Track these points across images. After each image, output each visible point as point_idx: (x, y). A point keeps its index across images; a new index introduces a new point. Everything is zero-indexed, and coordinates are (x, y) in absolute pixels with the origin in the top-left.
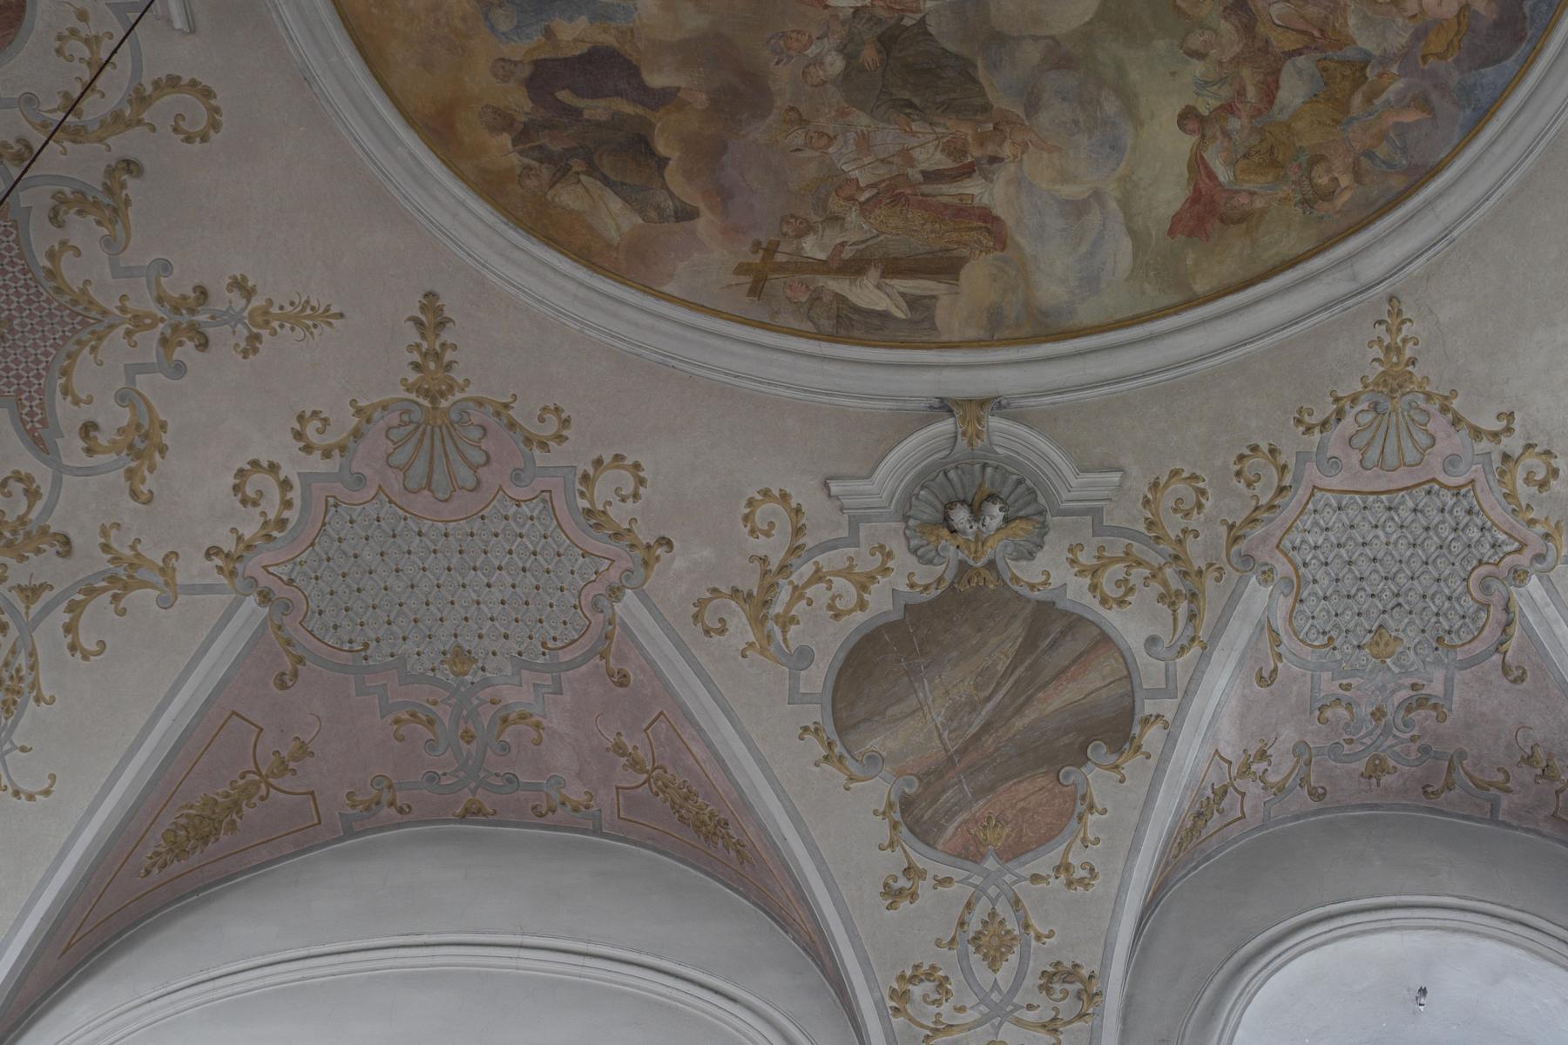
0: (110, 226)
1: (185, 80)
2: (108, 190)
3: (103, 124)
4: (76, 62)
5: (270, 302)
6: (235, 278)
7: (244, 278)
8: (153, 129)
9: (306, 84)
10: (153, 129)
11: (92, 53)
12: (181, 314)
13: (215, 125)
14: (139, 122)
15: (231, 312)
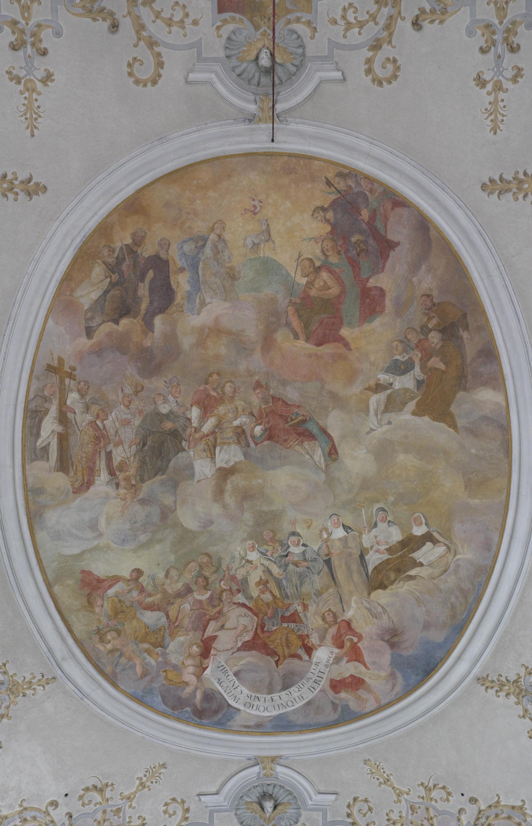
0: (81, 5)
1: (161, 71)
2: (102, 10)
3: (139, 17)
4: (171, 12)
5: (39, 94)
6: (52, 75)
7: (53, 80)
8: (136, 46)
9: (158, 138)
10: (136, 46)
11: (176, 22)
12: (31, 37)
13: (137, 82)
14: (139, 39)
15: (33, 69)
